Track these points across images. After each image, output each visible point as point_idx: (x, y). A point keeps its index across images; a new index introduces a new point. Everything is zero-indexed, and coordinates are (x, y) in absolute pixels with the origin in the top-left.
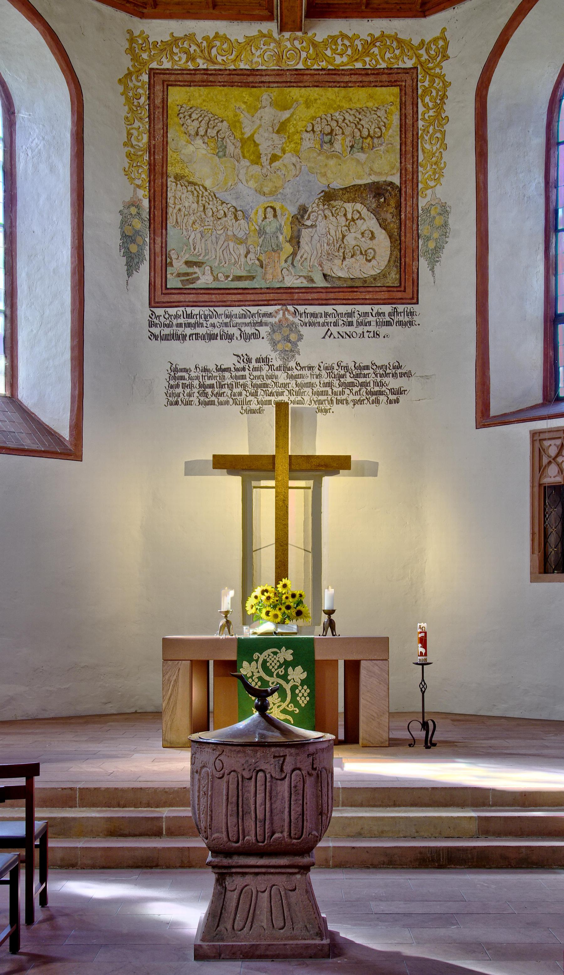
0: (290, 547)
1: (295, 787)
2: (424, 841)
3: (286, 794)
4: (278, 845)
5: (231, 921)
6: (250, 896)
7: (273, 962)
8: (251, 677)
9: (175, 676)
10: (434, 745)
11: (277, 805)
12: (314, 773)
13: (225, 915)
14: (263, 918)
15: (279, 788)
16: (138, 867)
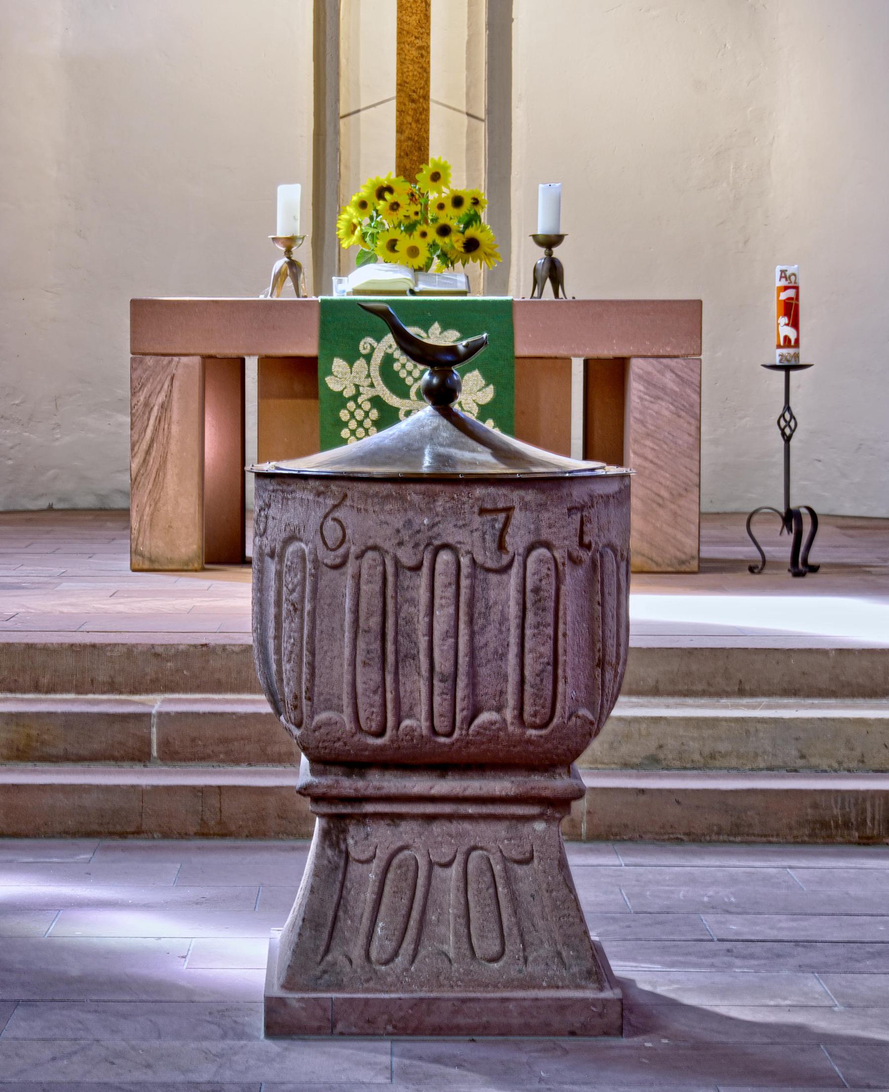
0: (433, 107)
1: (537, 590)
2: (822, 778)
3: (513, 610)
4: (490, 741)
5: (361, 940)
6: (411, 875)
7: (471, 1045)
8: (354, 398)
9: (163, 394)
10: (814, 569)
11: (489, 637)
12: (586, 556)
13: (345, 923)
14: (447, 936)
15: (492, 594)
16: (90, 835)
